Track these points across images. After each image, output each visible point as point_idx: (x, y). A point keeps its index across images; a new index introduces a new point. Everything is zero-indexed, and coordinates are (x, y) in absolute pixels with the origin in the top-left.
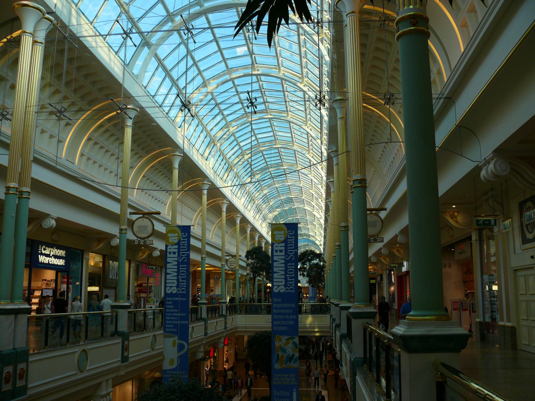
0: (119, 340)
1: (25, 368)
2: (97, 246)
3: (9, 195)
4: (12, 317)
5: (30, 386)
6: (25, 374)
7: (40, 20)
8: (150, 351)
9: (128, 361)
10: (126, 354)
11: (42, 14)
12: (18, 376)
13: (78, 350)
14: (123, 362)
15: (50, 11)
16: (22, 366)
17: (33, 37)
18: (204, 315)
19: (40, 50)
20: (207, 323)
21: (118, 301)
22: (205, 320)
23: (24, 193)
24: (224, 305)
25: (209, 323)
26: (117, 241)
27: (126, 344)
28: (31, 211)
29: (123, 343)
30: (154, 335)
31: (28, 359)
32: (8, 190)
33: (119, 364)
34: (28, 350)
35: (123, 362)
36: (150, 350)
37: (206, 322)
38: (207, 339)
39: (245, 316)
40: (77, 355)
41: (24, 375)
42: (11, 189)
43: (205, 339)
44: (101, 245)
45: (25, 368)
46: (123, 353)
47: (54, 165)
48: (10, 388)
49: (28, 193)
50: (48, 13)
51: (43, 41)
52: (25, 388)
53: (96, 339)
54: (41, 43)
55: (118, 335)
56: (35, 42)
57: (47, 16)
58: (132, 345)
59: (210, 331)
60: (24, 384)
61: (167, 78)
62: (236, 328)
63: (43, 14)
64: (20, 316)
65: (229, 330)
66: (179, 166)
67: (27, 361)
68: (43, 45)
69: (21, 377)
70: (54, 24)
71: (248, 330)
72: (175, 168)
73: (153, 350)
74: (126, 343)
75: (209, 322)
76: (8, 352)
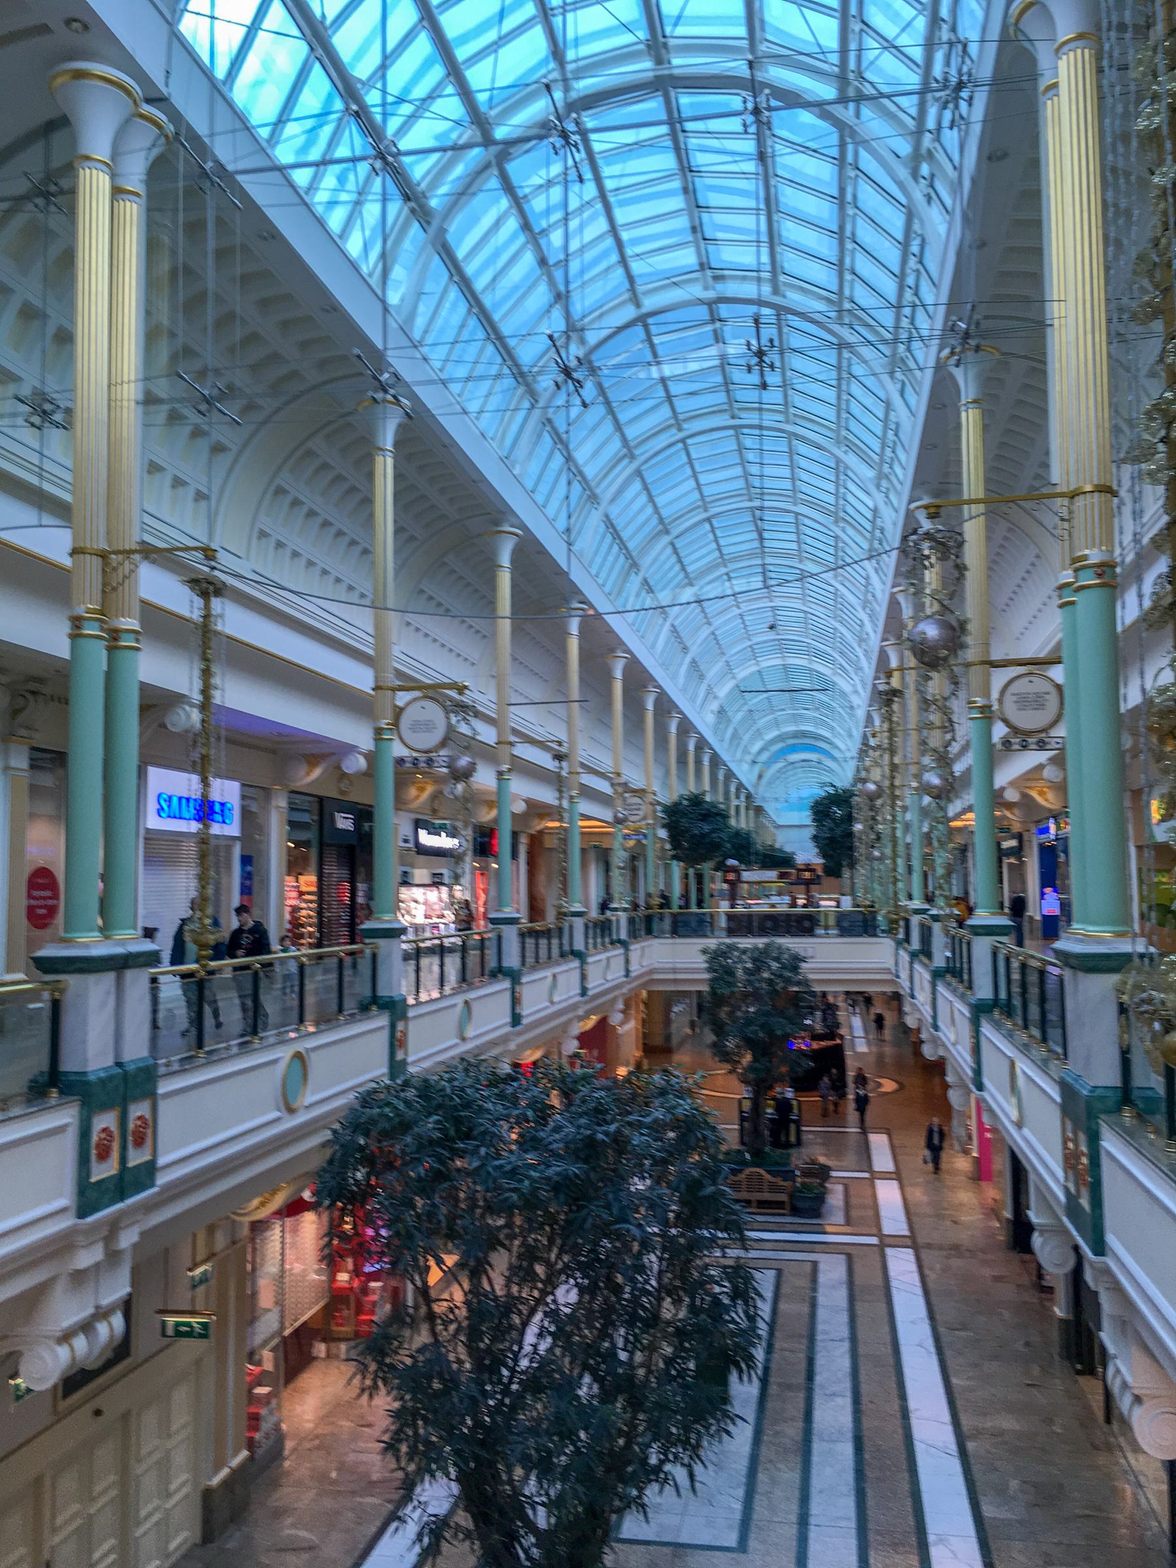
0: (383, 1021)
1: (148, 1116)
2: (308, 774)
3: (83, 642)
4: (109, 978)
5: (162, 1161)
6: (149, 1132)
7: (128, 121)
8: (277, 1120)
9: (153, 1185)
10: (400, 1056)
11: (130, 102)
12: (94, 1152)
13: (284, 1054)
14: (82, 1212)
15: (154, 95)
16: (139, 1110)
17: (113, 176)
18: (512, 959)
19: (132, 212)
20: (520, 984)
21: (379, 919)
22: (514, 977)
23: (123, 636)
24: (579, 923)
25: (169, 1095)
26: (188, 716)
28: (144, 687)
29: (393, 1026)
30: (298, 1056)
31: (155, 1088)
32: (78, 627)
33: (508, 1029)
34: (156, 1066)
35: (82, 1212)
36: (275, 1114)
37: (583, 962)
38: (586, 1003)
39: (670, 941)
40: (281, 1067)
41: (144, 1134)
42: (86, 623)
43: (81, 1240)
44: (317, 773)
45: (148, 1116)
47: (34, 480)
48: (113, 1172)
49: (132, 636)
50: (148, 101)
51: (141, 189)
52: (150, 1169)
53: (325, 1021)
54: (137, 195)
55: (62, 1092)
56: (117, 192)
57: (147, 109)
58: (634, 956)
59: (595, 983)
60: (148, 1157)
61: (317, 67)
62: (652, 971)
63: (135, 102)
64: (129, 974)
65: (637, 978)
66: (513, 562)
67: (152, 1095)
68: (143, 201)
69: (139, 1142)
70: (167, 137)
71: (679, 976)
72: (88, 158)
73: (463, 1039)
74: (400, 1026)
75: (524, 980)
76: (102, 1074)
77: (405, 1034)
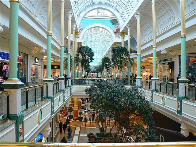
27: (21, 129)
46: (51, 110)
77: (23, 129)
